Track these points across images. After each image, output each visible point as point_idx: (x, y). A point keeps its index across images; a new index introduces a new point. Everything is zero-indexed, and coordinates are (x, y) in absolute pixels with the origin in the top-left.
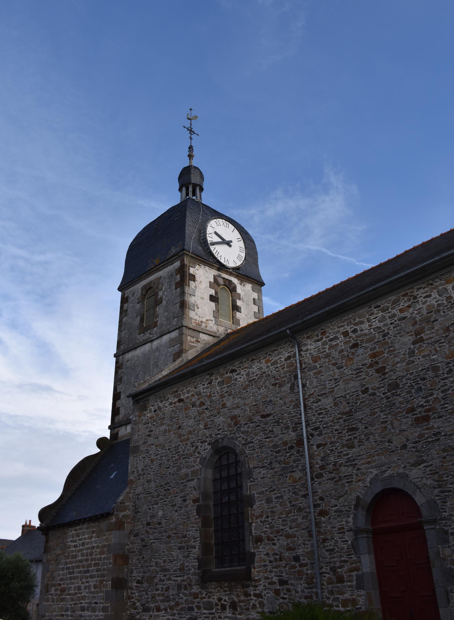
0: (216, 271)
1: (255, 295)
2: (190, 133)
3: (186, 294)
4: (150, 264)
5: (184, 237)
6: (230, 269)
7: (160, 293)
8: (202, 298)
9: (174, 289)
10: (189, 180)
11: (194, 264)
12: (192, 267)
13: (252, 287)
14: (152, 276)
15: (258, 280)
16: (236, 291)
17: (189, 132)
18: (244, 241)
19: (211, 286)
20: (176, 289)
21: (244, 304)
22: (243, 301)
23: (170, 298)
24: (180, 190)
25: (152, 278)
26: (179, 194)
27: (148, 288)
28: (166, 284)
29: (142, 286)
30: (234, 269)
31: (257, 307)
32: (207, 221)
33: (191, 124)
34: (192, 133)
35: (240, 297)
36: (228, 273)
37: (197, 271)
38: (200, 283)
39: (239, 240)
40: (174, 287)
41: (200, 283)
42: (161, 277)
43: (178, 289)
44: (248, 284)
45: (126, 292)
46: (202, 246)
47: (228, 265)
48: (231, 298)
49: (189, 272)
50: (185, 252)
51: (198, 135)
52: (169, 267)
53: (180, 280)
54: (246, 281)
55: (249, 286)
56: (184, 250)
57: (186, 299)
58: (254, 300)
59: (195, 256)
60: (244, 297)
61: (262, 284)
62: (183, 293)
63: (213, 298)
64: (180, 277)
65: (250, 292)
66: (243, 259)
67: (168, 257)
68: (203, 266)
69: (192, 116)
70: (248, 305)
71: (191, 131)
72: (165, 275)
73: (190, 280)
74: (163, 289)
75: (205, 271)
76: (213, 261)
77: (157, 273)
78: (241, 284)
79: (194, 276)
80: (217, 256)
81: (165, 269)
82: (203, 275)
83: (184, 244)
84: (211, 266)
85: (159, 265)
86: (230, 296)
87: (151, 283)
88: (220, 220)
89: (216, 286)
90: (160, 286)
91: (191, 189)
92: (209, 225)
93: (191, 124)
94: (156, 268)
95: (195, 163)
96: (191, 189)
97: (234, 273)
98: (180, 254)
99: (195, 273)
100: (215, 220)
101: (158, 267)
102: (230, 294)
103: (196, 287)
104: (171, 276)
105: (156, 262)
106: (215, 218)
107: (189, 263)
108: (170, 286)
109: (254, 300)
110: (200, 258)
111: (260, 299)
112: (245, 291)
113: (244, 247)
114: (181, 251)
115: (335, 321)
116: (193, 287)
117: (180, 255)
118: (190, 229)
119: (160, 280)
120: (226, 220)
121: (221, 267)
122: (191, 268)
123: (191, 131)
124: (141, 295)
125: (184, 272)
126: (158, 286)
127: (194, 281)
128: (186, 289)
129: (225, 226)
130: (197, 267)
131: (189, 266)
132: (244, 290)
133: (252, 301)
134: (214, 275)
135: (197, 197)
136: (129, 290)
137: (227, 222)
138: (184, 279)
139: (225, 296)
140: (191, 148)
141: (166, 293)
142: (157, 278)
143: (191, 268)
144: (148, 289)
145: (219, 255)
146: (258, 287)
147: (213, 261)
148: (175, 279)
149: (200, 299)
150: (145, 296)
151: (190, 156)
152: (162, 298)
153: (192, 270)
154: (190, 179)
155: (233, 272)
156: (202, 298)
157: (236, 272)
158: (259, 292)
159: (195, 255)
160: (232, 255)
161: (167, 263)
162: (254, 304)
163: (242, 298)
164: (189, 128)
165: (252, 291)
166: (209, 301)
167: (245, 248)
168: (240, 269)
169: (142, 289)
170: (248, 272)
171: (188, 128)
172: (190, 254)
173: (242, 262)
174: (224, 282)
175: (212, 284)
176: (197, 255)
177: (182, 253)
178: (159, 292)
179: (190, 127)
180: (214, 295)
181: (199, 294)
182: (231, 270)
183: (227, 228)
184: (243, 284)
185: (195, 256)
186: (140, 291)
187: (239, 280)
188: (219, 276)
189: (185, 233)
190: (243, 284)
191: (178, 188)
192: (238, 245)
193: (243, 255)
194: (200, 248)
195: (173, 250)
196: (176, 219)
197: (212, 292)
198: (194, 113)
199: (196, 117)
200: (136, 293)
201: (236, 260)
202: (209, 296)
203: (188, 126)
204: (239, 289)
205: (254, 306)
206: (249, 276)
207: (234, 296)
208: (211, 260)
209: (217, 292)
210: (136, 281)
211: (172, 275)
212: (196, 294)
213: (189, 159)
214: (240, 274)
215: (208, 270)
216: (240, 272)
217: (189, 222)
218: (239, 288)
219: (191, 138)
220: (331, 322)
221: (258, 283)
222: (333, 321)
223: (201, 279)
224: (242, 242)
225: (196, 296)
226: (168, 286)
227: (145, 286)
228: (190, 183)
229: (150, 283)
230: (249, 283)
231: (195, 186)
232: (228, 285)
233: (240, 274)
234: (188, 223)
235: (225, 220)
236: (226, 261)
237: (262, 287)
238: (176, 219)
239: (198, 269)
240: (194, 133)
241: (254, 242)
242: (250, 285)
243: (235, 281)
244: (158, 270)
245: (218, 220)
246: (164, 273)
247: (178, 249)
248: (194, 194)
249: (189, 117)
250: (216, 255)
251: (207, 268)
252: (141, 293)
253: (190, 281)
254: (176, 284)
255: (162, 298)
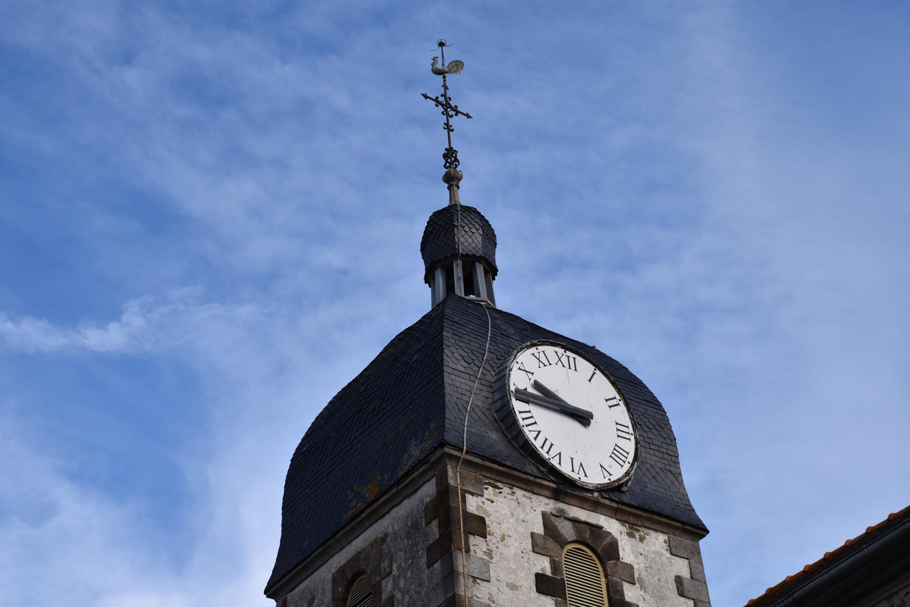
0: (547, 501)
1: (681, 567)
2: (445, 113)
3: (461, 578)
4: (351, 500)
5: (443, 407)
6: (591, 491)
7: (387, 586)
8: (513, 587)
9: (424, 566)
10: (455, 248)
11: (479, 483)
12: (473, 494)
13: (669, 543)
14: (361, 537)
15: (683, 519)
16: (617, 557)
17: (440, 109)
18: (627, 405)
19: (537, 548)
20: (430, 565)
21: (647, 597)
22: (642, 587)
23: (415, 596)
24: (429, 279)
25: (359, 543)
26: (427, 290)
27: (349, 577)
28: (402, 554)
29: (333, 571)
30: (603, 490)
31: (691, 603)
32: (509, 354)
33: (446, 88)
34: (452, 113)
35: (632, 576)
36: (586, 505)
37: (488, 506)
38: (503, 539)
39: (614, 402)
40: (424, 560)
41: (503, 539)
42: (386, 535)
43: (437, 565)
44: (653, 534)
45: (289, 596)
46: (499, 430)
47: (584, 479)
48: (603, 580)
49: (464, 510)
50: (447, 450)
51: (468, 116)
52: (405, 502)
53: (440, 536)
54: (647, 524)
55: (657, 541)
56: (443, 444)
57: (461, 591)
58: (679, 580)
59: (479, 461)
60: (644, 574)
61: (698, 531)
62: (450, 576)
63: (544, 585)
64: (440, 526)
65: (664, 559)
66: (631, 458)
67: (401, 473)
68: (506, 490)
69: (446, 64)
70: (661, 599)
71: (447, 107)
72: (396, 528)
73: (468, 532)
74: (395, 572)
75: (514, 504)
76: (536, 472)
77: (375, 526)
78: (630, 535)
79: (482, 520)
80: (547, 456)
81: (396, 509)
82: (510, 518)
83: (442, 428)
84: (531, 486)
85: (378, 499)
86: (602, 574)
87: (358, 560)
88: (550, 350)
89: (551, 545)
90: (385, 565)
91: (458, 272)
92: (515, 367)
93: (446, 88)
94: (369, 511)
95: (465, 197)
96: (458, 272)
97: (607, 502)
98: (432, 460)
99: (486, 512)
100: (533, 350)
101: (375, 505)
102: (601, 569)
103: (489, 553)
104: (413, 528)
105: (369, 491)
106: (533, 345)
107: (462, 484)
108: (413, 558)
109: (679, 580)
110: (496, 466)
111: (698, 577)
112: (646, 557)
113: (628, 422)
114: (436, 449)
115: (903, 593)
116: (480, 554)
117: (433, 464)
118: (461, 382)
119: (385, 546)
120: (566, 349)
121: (564, 487)
122: (469, 497)
123: (447, 107)
124: (334, 600)
125: (448, 509)
126: (379, 564)
127: (484, 535)
128: (460, 562)
129: (566, 365)
130: (489, 492)
131: (464, 492)
132: (644, 552)
133: (673, 586)
134: (544, 515)
135: (478, 295)
136: (297, 590)
137: (568, 353)
138: (451, 529)
139: (585, 577)
140: (450, 155)
141: (402, 583)
142: (375, 541)
143: (469, 497)
144: (349, 577)
145: (553, 452)
146: (687, 541)
147: (536, 472)
148: (426, 536)
149: (507, 590)
150: (345, 600)
151: (452, 180)
152: (391, 598)
153: (473, 504)
154: (452, 243)
155: (602, 501)
156: (513, 587)
157: (610, 500)
158: (694, 557)
159: (477, 455)
160: (596, 451)
161: (399, 492)
162: (681, 594)
163: (640, 580)
164: (441, 99)
165: (668, 555)
166: (534, 594)
167: (634, 426)
168: (625, 489)
169: (334, 580)
170: (655, 500)
171: (436, 100)
172: (464, 456)
173: (627, 466)
174: (578, 532)
175: (540, 542)
176: (484, 458)
177: (438, 454)
178: (384, 584)
179: (444, 95)
180: (548, 572)
181: (502, 576)
182: (596, 494)
183: (572, 371)
184: (637, 535)
185: (479, 461)
186: (329, 587)
187: (623, 522)
188: (561, 514)
189: (443, 396)
190: (637, 535)
191: (423, 273)
192: (612, 417)
193: (630, 446)
194: (494, 436)
195: (415, 451)
196: (415, 358)
197: (544, 565)
198: (451, 54)
199: (457, 66)
200: (319, 596)
201: (608, 463)
202: (533, 578)
203: (436, 91)
204: (628, 551)
205: (682, 599)
206: (656, 509)
207: (613, 574)
208: (531, 468)
209: (559, 563)
210: (316, 557)
211: (416, 526)
212: (492, 574)
213: (449, 188)
214: (624, 504)
215: (522, 500)
216: (625, 499)
217: (454, 361)
218: (628, 549)
219: (448, 128)
220: (889, 598)
221: (687, 529)
222: (896, 593)
223: (504, 526)
224: (622, 407)
225: (493, 580)
226: (406, 560)
227: (342, 570)
228: (455, 255)
229: (354, 560)
230: (657, 531)
231: (470, 261)
232: (589, 541)
233: (624, 504)
234: (451, 365)
235: (563, 347)
236: (576, 468)
237: (701, 542)
238: (415, 358)
239: (492, 497)
240: (457, 113)
241: (660, 405)
242: (662, 537)
243: (612, 526)
244: (375, 516)
245: (541, 348)
246: (391, 522)
247: (428, 444)
248: (470, 286)
249: (439, 66)
250: (543, 452)
251: (520, 493)
252: (333, 592)
253: (471, 538)
254: (430, 549)
255: (391, 598)
